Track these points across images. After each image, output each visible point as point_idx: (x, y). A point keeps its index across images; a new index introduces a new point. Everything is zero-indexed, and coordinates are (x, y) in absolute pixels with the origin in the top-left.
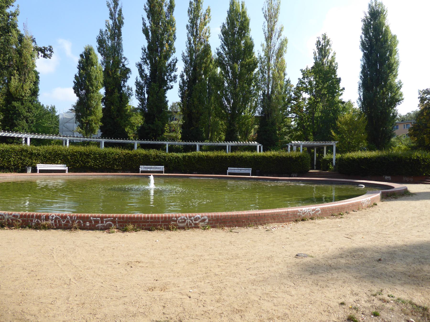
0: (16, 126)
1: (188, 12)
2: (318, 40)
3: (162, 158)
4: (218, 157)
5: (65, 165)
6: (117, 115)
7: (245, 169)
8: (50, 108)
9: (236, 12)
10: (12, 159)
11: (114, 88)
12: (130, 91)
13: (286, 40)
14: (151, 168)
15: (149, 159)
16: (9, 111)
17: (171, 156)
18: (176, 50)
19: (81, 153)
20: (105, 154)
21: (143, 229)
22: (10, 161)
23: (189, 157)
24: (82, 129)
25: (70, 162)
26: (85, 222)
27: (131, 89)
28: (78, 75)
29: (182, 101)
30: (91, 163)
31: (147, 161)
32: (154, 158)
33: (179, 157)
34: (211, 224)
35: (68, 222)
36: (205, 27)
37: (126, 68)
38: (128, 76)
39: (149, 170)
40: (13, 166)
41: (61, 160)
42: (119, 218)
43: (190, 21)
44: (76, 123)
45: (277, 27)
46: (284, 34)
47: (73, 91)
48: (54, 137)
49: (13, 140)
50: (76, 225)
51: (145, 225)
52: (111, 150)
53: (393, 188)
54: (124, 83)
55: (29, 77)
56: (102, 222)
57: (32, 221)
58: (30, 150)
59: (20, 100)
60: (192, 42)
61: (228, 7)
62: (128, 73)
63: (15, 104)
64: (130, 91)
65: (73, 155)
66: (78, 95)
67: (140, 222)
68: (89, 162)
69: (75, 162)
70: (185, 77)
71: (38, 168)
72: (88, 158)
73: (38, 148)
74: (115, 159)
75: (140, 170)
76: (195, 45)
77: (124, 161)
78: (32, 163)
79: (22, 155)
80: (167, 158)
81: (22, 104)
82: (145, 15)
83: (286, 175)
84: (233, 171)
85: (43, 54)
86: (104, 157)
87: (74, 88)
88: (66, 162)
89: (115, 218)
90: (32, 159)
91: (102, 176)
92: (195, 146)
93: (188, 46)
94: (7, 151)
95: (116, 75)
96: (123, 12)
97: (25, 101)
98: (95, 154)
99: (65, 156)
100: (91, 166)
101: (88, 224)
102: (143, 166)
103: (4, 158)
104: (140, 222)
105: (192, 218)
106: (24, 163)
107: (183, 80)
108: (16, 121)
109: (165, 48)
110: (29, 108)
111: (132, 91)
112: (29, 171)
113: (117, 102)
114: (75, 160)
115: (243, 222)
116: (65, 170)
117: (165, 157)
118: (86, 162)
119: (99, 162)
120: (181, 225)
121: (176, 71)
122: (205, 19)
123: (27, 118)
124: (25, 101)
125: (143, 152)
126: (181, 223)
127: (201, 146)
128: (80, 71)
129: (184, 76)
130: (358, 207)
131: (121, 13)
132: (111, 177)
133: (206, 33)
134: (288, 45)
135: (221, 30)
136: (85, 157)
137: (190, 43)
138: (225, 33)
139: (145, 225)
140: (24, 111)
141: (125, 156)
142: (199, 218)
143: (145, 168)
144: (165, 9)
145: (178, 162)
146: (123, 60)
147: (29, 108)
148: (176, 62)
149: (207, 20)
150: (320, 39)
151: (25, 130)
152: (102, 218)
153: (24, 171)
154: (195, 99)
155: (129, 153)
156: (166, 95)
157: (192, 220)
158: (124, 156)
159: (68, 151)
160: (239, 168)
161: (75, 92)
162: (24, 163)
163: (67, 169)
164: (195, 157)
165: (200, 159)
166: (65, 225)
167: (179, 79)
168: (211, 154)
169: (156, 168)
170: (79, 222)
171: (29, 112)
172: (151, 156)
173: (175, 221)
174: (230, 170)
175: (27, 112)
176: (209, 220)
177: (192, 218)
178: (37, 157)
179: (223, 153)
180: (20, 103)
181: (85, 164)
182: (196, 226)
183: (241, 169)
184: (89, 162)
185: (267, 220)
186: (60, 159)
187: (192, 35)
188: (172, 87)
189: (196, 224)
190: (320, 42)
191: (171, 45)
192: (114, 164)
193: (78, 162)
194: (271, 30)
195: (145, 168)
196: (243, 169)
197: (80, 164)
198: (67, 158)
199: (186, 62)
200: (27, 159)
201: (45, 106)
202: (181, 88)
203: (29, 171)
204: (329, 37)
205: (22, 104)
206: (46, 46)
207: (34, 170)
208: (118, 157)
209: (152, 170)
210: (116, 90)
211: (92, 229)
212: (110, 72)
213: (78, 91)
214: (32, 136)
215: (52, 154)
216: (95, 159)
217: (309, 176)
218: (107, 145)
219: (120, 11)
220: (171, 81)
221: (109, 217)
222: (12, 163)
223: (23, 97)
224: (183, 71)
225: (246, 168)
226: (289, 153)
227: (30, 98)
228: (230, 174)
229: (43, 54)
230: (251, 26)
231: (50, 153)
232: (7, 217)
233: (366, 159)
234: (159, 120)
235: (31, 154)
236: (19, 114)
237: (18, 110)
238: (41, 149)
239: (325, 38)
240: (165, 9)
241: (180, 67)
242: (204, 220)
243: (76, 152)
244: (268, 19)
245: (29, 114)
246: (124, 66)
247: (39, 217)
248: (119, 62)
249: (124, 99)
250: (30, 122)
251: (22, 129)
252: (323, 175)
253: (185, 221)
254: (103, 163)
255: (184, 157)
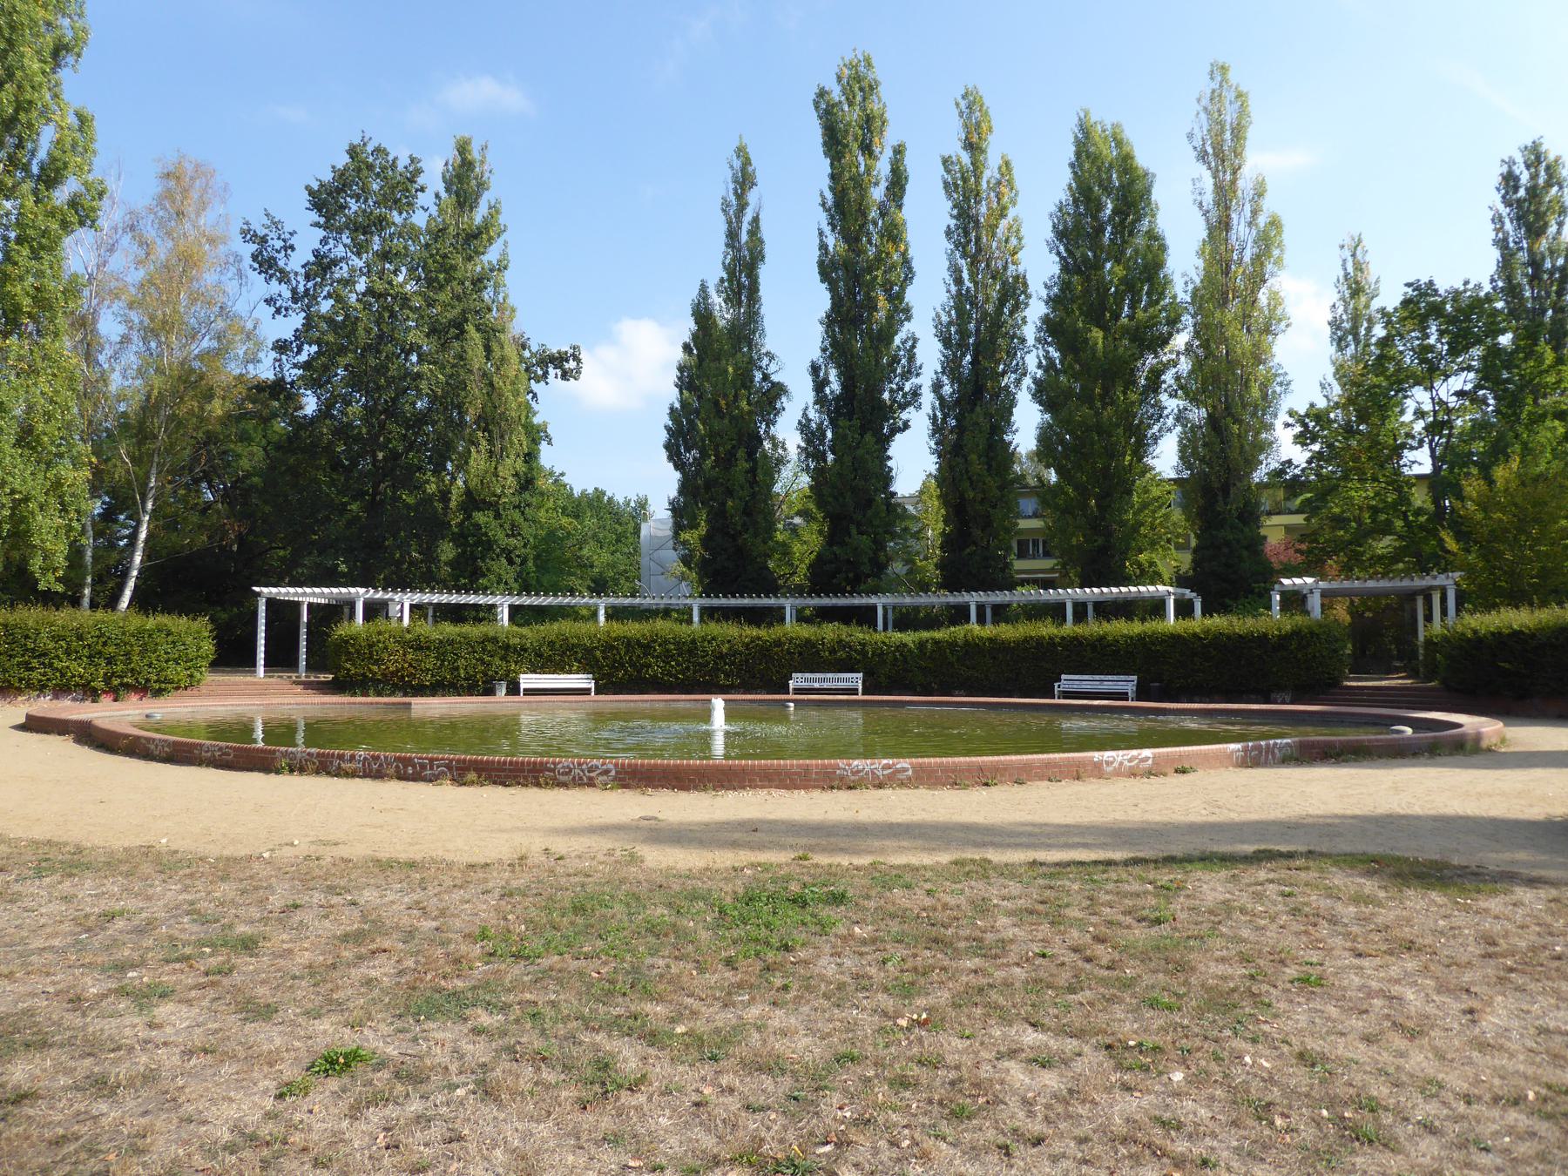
0: (484, 576)
1: (945, 188)
2: (1505, 169)
3: (856, 651)
4: (1027, 640)
5: (591, 676)
6: (744, 524)
7: (1115, 678)
8: (633, 504)
9: (1095, 159)
10: (462, 662)
11: (733, 447)
12: (780, 451)
13: (1275, 223)
14: (824, 680)
15: (818, 652)
16: (466, 538)
17: (883, 643)
18: (914, 311)
19: (629, 641)
20: (693, 641)
21: (495, 783)
22: (457, 669)
23: (936, 642)
24: (690, 569)
25: (601, 668)
26: (405, 767)
27: (784, 443)
28: (677, 405)
29: (939, 470)
30: (656, 669)
31: (812, 658)
32: (833, 651)
33: (905, 645)
34: (620, 780)
35: (381, 765)
36: (1003, 224)
37: (774, 384)
38: (778, 405)
39: (817, 685)
40: (466, 679)
41: (580, 662)
42: (458, 761)
43: (955, 212)
44: (675, 549)
45: (1245, 183)
46: (1269, 205)
47: (664, 454)
48: (567, 600)
49: (477, 611)
50: (391, 771)
51: (499, 777)
52: (714, 628)
53: (1459, 726)
54: (768, 426)
55: (511, 443)
56: (432, 768)
57: (331, 762)
58: (502, 637)
59: (493, 507)
60: (965, 275)
61: (1070, 153)
62: (778, 396)
63: (480, 517)
64: (780, 451)
65: (608, 647)
66: (679, 466)
67: (492, 770)
68: (649, 666)
69: (613, 666)
70: (947, 390)
71: (523, 686)
72: (645, 655)
73: (525, 631)
74: (722, 656)
75: (791, 687)
76: (976, 283)
77: (747, 661)
78: (509, 671)
79: (484, 650)
80: (869, 649)
81: (498, 516)
82: (822, 218)
83: (1253, 697)
84: (1075, 687)
85: (559, 372)
86: (690, 651)
87: (667, 447)
88: (592, 667)
89: (451, 761)
90: (507, 662)
91: (662, 705)
92: (874, 608)
93: (953, 289)
94: (451, 642)
95: (738, 407)
96: (762, 224)
97: (504, 509)
98: (666, 642)
99: (589, 651)
100: (655, 676)
101: (410, 770)
102: (799, 675)
103: (443, 661)
104: (492, 770)
105: (584, 767)
106: (490, 673)
107: (941, 398)
108: (483, 561)
109: (881, 315)
110: (513, 525)
111: (785, 450)
112: (502, 690)
113: (742, 488)
114: (615, 661)
115: (690, 780)
116: (589, 689)
117: (864, 645)
118: (643, 666)
119: (678, 665)
120: (563, 778)
121: (918, 375)
122: (999, 197)
123: (510, 552)
124: (504, 509)
125: (806, 631)
126: (562, 774)
127: (981, 608)
128: (681, 393)
129: (941, 387)
130: (1098, 771)
131: (758, 227)
132: (688, 705)
133: (1007, 241)
134: (1287, 236)
135: (1054, 227)
136: (639, 652)
137: (959, 281)
138: (1063, 234)
139: (499, 777)
140: (500, 535)
141: (748, 645)
142: (597, 767)
143: (807, 680)
144: (878, 193)
145: (905, 661)
146: (765, 361)
147: (513, 525)
148: (913, 347)
149: (1006, 199)
150: (1515, 168)
151: (506, 583)
152: (432, 760)
153: (490, 692)
154: (974, 457)
155: (759, 638)
156: (890, 453)
157: (583, 771)
158: (747, 646)
159: (595, 635)
160: (1097, 677)
161: (670, 458)
162: (490, 673)
163: (592, 685)
164: (957, 645)
165: (972, 648)
166: (378, 771)
167: (928, 399)
168: (1007, 632)
169: (839, 680)
170: (397, 767)
171: (513, 536)
172: (823, 644)
173: (553, 770)
174: (1068, 681)
175: (507, 535)
176: (617, 773)
177: (584, 767)
178: (519, 655)
179: (1046, 629)
180: (491, 514)
181: (639, 672)
182: (591, 784)
183: (1102, 677)
184: (649, 666)
185: (750, 781)
186: (576, 660)
187: (964, 255)
188: (906, 426)
189: (591, 779)
190: (1517, 179)
191: (896, 299)
192: (718, 669)
193: (622, 665)
194: (1225, 194)
195: (807, 680)
196: (1110, 678)
197: (626, 671)
198: (595, 657)
199: (946, 341)
200: (498, 662)
201: (620, 499)
202: (937, 429)
203: (502, 690)
204: (1552, 150)
205: (498, 516)
206: (563, 350)
207: (514, 689)
208: (730, 649)
209: (826, 685)
210: (741, 453)
211: (414, 780)
212: (723, 402)
213: (679, 454)
214: (612, 600)
215: (557, 646)
216: (667, 656)
217: (1335, 700)
218: (708, 613)
219: (756, 220)
220: (903, 407)
221: (443, 759)
222: (462, 671)
223: (499, 497)
224: (939, 370)
225: (1118, 674)
226: (1274, 619)
227: (516, 500)
228: (1067, 695)
229: (559, 372)
230: (1156, 195)
231: (551, 644)
232: (299, 755)
233: (1517, 635)
234: (862, 533)
235: (507, 647)
236: (489, 545)
237: (486, 534)
238: (531, 634)
239: (1535, 155)
240: (878, 193)
241: (930, 356)
242: (606, 772)
243: (616, 639)
244: (1213, 164)
245: (513, 541)
246: (766, 377)
247: (341, 757)
248: (752, 364)
249: (760, 477)
250: (518, 560)
251: (498, 583)
252: (1388, 695)
253: (571, 771)
254: (688, 668)
255: (922, 645)
